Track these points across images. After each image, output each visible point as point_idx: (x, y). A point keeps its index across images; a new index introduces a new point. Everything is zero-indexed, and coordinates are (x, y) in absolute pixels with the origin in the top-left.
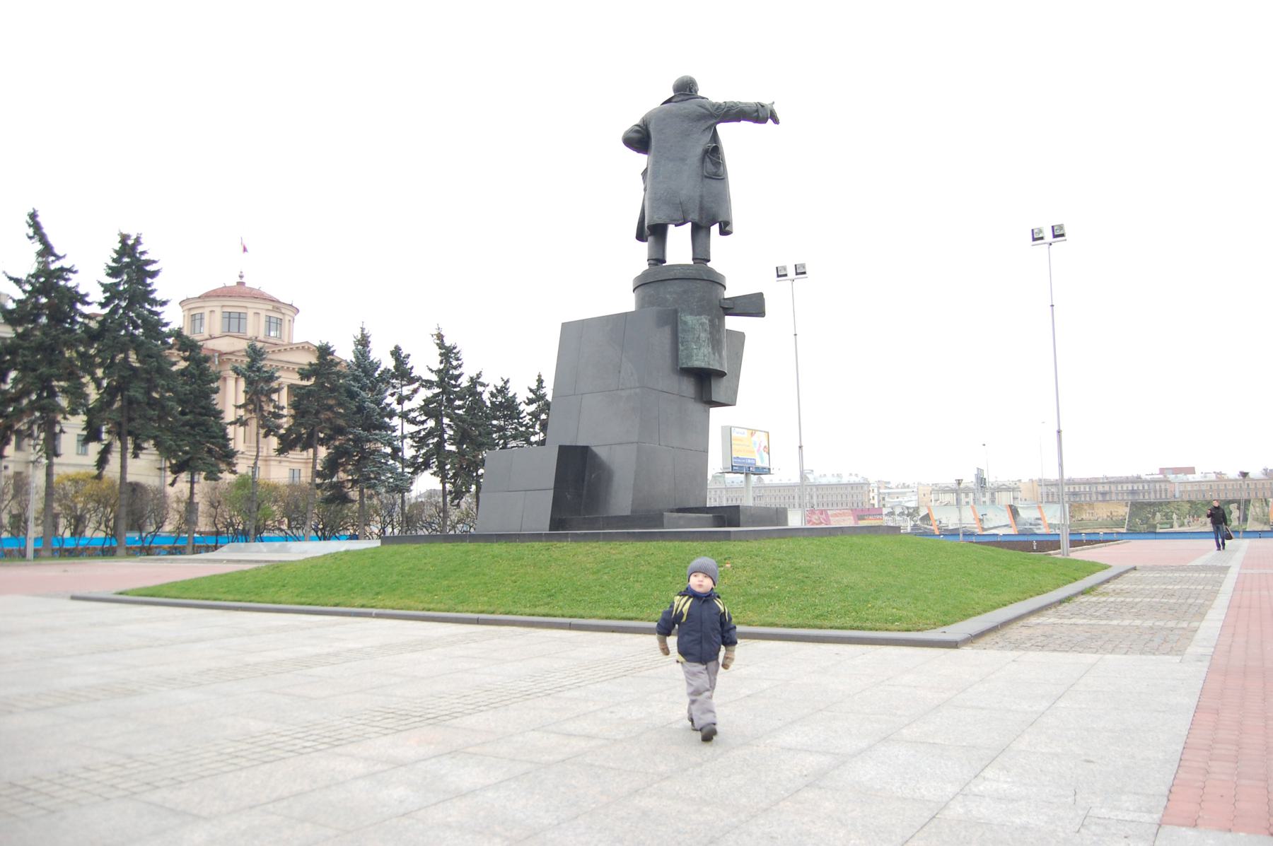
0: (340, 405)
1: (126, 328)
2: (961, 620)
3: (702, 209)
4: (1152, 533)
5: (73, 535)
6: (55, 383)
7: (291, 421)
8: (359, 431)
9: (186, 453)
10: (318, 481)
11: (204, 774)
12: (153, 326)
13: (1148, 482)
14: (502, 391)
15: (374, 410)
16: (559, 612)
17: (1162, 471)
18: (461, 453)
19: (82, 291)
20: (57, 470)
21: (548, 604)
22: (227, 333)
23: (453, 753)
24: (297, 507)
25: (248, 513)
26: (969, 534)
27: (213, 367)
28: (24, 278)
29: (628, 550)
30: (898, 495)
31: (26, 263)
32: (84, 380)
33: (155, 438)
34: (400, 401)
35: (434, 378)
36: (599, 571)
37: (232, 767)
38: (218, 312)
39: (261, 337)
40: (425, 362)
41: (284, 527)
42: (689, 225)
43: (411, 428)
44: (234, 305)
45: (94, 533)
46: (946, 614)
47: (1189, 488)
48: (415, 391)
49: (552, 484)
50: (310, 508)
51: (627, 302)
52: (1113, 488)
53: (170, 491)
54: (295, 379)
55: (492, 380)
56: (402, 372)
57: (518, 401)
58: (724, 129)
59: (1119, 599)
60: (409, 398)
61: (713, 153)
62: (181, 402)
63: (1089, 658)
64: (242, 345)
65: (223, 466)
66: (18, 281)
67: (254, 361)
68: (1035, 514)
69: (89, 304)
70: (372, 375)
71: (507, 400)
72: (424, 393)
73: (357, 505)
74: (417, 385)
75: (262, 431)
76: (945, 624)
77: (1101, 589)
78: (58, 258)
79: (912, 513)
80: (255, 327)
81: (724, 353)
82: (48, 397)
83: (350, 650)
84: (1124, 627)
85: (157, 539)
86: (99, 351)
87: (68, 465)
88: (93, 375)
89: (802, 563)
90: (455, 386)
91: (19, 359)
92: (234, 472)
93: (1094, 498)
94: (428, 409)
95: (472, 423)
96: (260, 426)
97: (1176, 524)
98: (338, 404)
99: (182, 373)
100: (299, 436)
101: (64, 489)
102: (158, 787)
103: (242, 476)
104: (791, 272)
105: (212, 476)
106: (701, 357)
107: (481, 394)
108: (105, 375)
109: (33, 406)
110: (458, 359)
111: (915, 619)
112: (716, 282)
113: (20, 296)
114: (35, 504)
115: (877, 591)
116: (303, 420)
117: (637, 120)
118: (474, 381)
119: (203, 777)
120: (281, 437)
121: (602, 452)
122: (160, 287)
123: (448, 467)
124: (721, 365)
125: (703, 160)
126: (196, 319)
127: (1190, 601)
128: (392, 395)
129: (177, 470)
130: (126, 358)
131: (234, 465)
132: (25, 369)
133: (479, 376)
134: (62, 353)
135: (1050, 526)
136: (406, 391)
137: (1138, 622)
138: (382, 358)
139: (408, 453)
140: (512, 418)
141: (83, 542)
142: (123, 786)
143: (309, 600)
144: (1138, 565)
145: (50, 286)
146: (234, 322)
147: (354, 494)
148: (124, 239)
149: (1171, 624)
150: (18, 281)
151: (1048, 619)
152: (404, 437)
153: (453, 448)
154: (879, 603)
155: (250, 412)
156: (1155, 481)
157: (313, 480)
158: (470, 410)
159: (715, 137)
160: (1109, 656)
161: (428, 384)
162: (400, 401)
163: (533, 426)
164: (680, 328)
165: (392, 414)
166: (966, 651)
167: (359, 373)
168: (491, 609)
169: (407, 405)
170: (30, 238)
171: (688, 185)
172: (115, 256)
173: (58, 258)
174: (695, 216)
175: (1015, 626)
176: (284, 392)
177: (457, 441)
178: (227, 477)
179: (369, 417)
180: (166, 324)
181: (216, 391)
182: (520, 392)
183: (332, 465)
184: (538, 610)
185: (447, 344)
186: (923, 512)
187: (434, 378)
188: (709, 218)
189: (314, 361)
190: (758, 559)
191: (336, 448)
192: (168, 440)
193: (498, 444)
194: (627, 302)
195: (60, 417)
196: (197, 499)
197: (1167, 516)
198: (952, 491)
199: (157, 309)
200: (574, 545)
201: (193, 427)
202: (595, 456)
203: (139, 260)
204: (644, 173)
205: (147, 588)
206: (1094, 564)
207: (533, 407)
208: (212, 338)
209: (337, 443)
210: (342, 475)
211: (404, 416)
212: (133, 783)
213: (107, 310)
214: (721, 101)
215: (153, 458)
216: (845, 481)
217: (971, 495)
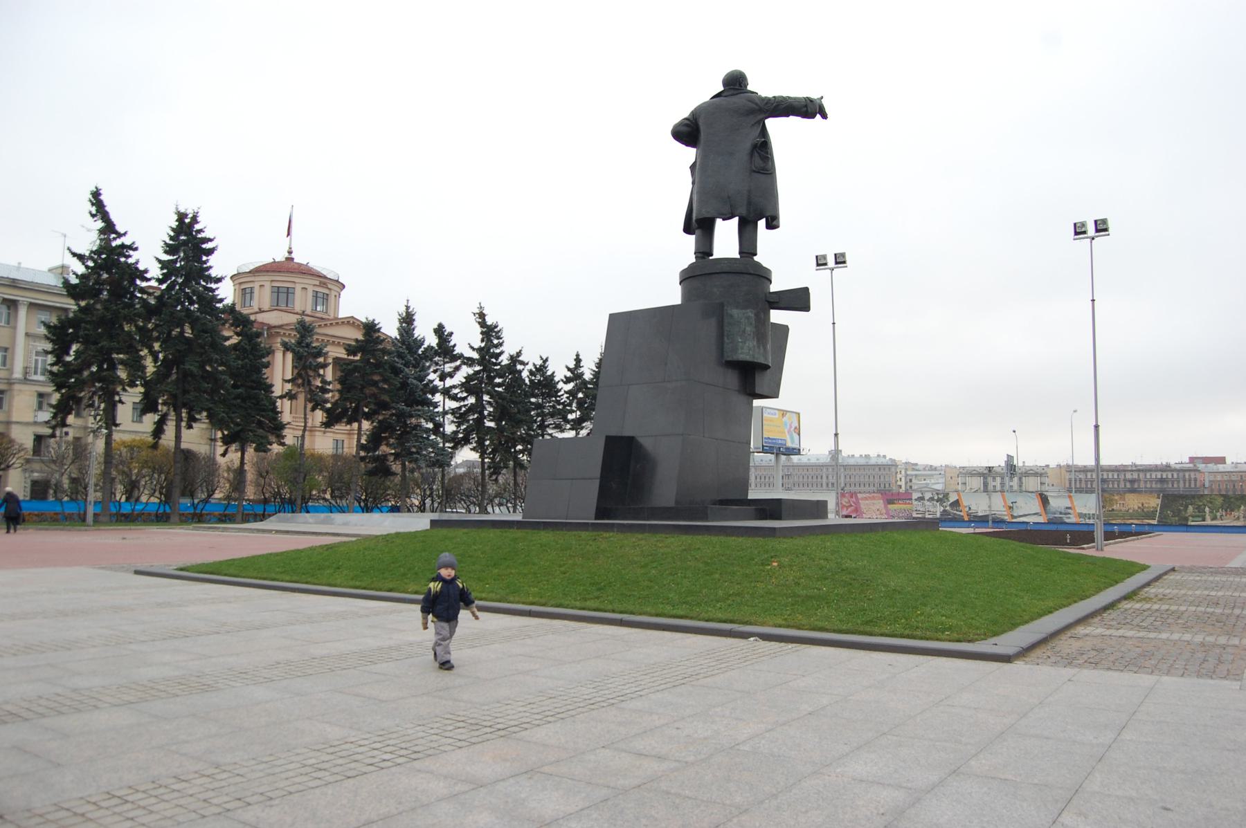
0: (385, 381)
1: (182, 304)
2: (1011, 629)
3: (749, 203)
4: (1183, 526)
5: (128, 499)
6: (115, 356)
7: (337, 396)
8: (402, 406)
9: (237, 424)
10: (362, 454)
11: (292, 789)
12: (208, 301)
13: (1178, 471)
14: (541, 369)
15: (417, 387)
16: (610, 607)
17: (1192, 460)
18: (500, 429)
19: (141, 267)
20: (117, 437)
21: (598, 598)
22: (275, 307)
23: (530, 772)
24: (341, 476)
25: (293, 482)
26: (998, 521)
27: (263, 341)
28: (87, 254)
29: (675, 543)
30: (925, 477)
31: (88, 240)
32: (142, 353)
33: (208, 410)
34: (442, 378)
35: (475, 355)
36: (646, 566)
37: (318, 782)
38: (268, 286)
39: (308, 312)
40: (467, 340)
41: (328, 496)
42: (736, 220)
43: (453, 405)
44: (283, 280)
45: (148, 499)
46: (995, 622)
47: (1219, 478)
48: (457, 369)
49: (598, 475)
50: (354, 479)
51: (672, 295)
52: (1142, 475)
53: (220, 459)
54: (341, 353)
55: (531, 358)
56: (445, 348)
57: (556, 379)
58: (772, 124)
59: (1165, 607)
60: (451, 375)
61: (762, 148)
62: (233, 375)
63: (1146, 680)
64: (293, 319)
65: (272, 438)
66: (81, 257)
67: (303, 337)
68: (1066, 503)
69: (148, 280)
70: (416, 352)
71: (546, 378)
72: (466, 371)
73: (398, 479)
74: (458, 363)
75: (310, 406)
76: (995, 634)
77: (1143, 593)
78: (120, 235)
79: (942, 498)
80: (302, 301)
81: (769, 347)
82: (107, 369)
83: (411, 644)
84: (1175, 643)
85: (208, 507)
86: (157, 326)
87: (124, 432)
88: (150, 348)
89: (848, 564)
90: (496, 364)
91: (81, 333)
92: (283, 444)
93: (1122, 485)
94: (469, 386)
95: (512, 399)
96: (307, 400)
97: (1208, 517)
98: (383, 375)
99: (235, 347)
100: (345, 411)
101: (120, 455)
102: (249, 804)
103: (289, 447)
104: (831, 262)
105: (262, 448)
106: (745, 350)
107: (520, 372)
108: (163, 349)
109: (95, 377)
110: (499, 338)
111: (965, 629)
112: (763, 276)
113: (81, 269)
114: (95, 469)
115: (924, 596)
116: (349, 395)
117: (686, 113)
118: (515, 359)
119: (291, 793)
120: (327, 411)
121: (647, 443)
122: (219, 264)
123: (487, 443)
124: (766, 359)
125: (751, 154)
126: (245, 293)
127: (1237, 611)
128: (435, 372)
129: (227, 441)
130: (182, 332)
131: (283, 437)
132: (86, 341)
133: (519, 354)
134: (121, 327)
135: (1081, 515)
136: (448, 368)
137: (1187, 637)
138: (425, 333)
139: (449, 428)
140: (550, 396)
141: (139, 507)
142: (215, 801)
143: (364, 584)
144: (1177, 565)
145: (111, 261)
146: (282, 296)
147: (396, 467)
148: (181, 217)
149: (1222, 640)
150: (81, 257)
151: (1094, 629)
152: (445, 413)
153: (492, 424)
154: (928, 609)
155: (299, 386)
156: (1184, 471)
157: (358, 453)
158: (509, 387)
159: (764, 132)
160: (1165, 678)
161: (469, 362)
162: (442, 378)
163: (570, 405)
164: (726, 321)
165: (434, 390)
166: (1018, 666)
167: (404, 350)
168: (543, 601)
169: (449, 382)
170: (93, 216)
171: (737, 180)
172: (172, 234)
173: (120, 235)
174: (744, 212)
175: (1063, 637)
176: (330, 369)
177: (497, 419)
178: (276, 448)
179: (412, 393)
180: (221, 300)
181: (267, 365)
182: (558, 369)
183: (376, 438)
184: (588, 604)
185: (489, 321)
186: (953, 498)
187: (475, 355)
188: (758, 209)
189: (361, 337)
190: (804, 558)
191: (380, 422)
192: (221, 412)
193: (535, 421)
194: (672, 295)
195: (119, 389)
196: (246, 467)
197: (1200, 510)
198: (980, 474)
199: (213, 286)
200: (621, 536)
201: (244, 400)
202: (637, 442)
203: (195, 238)
204: (693, 167)
205: (207, 565)
206: (1133, 564)
207: (570, 386)
208: (261, 311)
209: (381, 418)
210: (384, 449)
211: (446, 392)
212: (226, 799)
213: (164, 287)
214: (770, 96)
215: (204, 426)
216: (873, 462)
217: (998, 479)
